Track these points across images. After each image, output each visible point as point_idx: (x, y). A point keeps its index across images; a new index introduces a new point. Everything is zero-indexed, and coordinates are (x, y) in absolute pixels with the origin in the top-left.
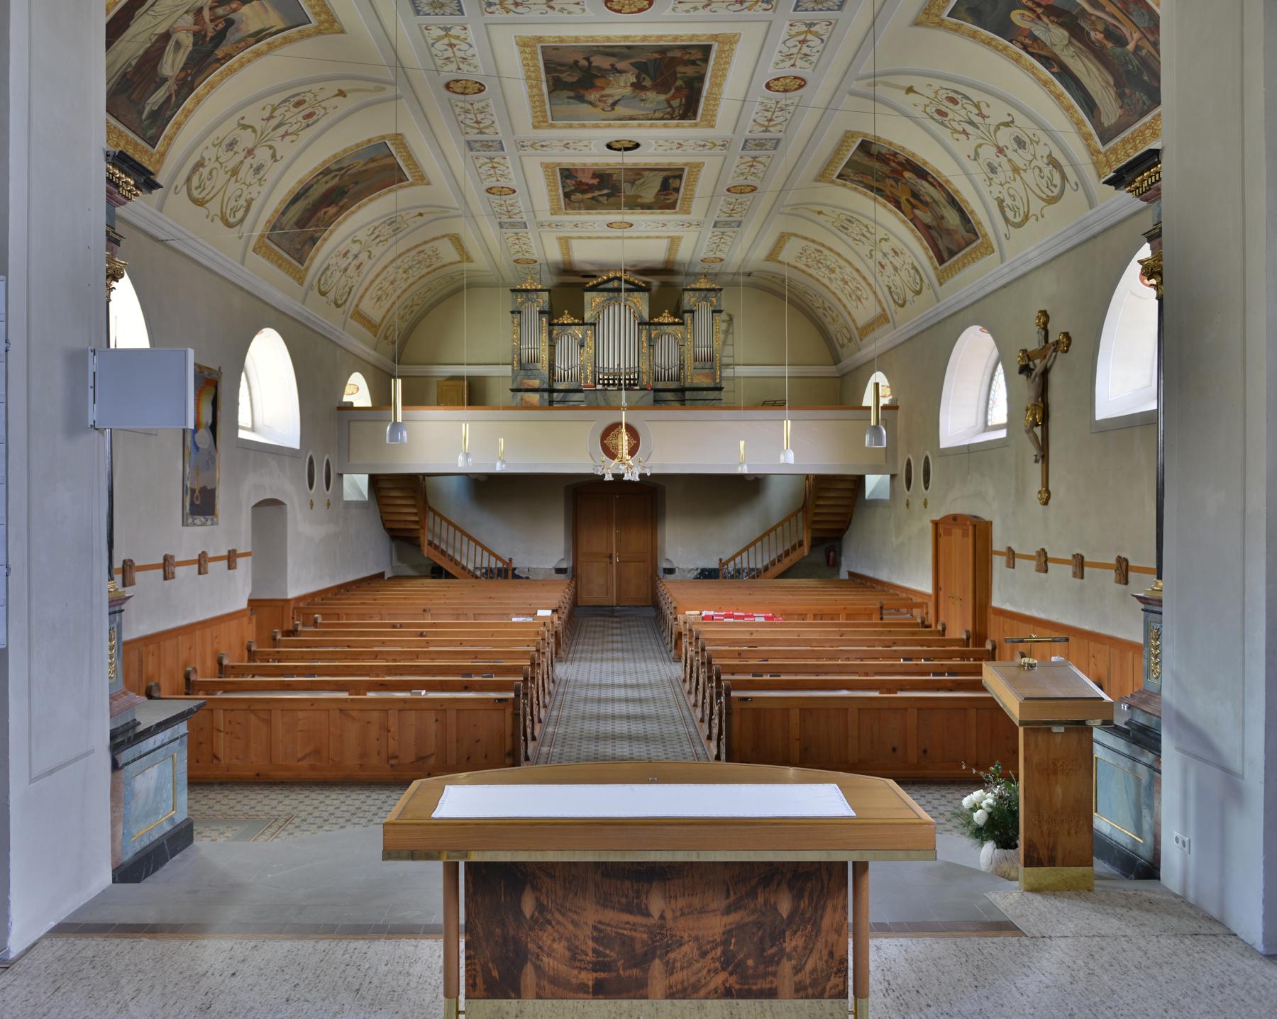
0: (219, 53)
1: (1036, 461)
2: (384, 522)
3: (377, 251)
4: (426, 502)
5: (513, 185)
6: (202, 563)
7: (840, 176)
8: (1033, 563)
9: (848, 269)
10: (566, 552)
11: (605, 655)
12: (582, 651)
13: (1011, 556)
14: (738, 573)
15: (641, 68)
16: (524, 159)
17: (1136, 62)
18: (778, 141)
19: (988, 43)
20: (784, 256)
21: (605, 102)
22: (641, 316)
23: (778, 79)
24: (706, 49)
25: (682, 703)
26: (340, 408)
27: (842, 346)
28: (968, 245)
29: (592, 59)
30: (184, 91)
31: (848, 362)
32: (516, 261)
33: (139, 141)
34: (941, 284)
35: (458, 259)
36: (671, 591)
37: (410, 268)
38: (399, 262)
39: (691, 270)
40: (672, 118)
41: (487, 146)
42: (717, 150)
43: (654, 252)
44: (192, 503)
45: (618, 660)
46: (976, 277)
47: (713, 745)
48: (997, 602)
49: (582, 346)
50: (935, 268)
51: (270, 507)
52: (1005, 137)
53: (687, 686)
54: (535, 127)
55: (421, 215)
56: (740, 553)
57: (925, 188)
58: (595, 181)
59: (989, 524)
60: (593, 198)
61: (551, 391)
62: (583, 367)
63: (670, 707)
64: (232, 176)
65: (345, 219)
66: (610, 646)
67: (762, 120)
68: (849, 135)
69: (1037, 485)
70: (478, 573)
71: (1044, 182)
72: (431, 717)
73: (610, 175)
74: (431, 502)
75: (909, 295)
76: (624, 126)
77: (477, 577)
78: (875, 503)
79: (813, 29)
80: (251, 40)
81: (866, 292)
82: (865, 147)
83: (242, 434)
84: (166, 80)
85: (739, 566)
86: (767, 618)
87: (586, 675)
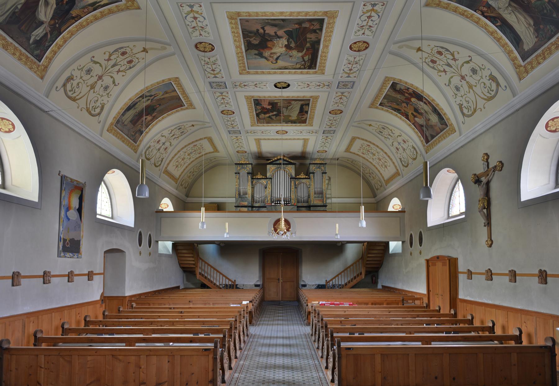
0: (74, 13)
1: (485, 226)
2: (180, 264)
3: (174, 142)
4: (198, 255)
5: (233, 109)
6: (70, 276)
7: (381, 104)
8: (484, 277)
9: (382, 153)
10: (259, 277)
11: (274, 323)
12: (264, 321)
13: (470, 274)
14: (334, 286)
15: (289, 34)
16: (237, 93)
17: (549, 7)
18: (354, 82)
19: (462, 14)
20: (354, 149)
21: (272, 57)
22: (291, 175)
23: (355, 43)
24: (321, 21)
25: (311, 347)
26: (157, 212)
27: (377, 189)
28: (441, 131)
29: (265, 28)
30: (56, 33)
31: (380, 196)
32: (238, 152)
33: (29, 55)
34: (427, 153)
35: (212, 150)
36: (304, 293)
37: (191, 153)
38: (184, 150)
39: (313, 157)
40: (305, 68)
41: (235, 132)
42: (325, 88)
43: (296, 147)
44: (64, 246)
45: (280, 324)
46: (446, 145)
47: (329, 373)
48: (461, 295)
49: (266, 188)
50: (424, 146)
51: (113, 253)
52: (466, 71)
53: (313, 338)
54: (240, 74)
55: (193, 126)
56: (335, 278)
57: (422, 106)
58: (270, 107)
59: (456, 260)
60: (269, 117)
61: (252, 207)
62: (266, 197)
63: (305, 349)
64: (91, 89)
65: (156, 123)
66: (277, 318)
67: (347, 70)
68: (387, 79)
69: (485, 237)
70: (221, 287)
71: (486, 90)
72: (166, 359)
73: (276, 103)
74: (201, 256)
75: (410, 161)
76: (282, 73)
77: (220, 288)
78: (394, 255)
79: (375, 8)
80: (91, 8)
81: (389, 163)
82: (394, 86)
83: (98, 217)
84: (42, 23)
85: (334, 283)
86: (350, 305)
87: (264, 333)
